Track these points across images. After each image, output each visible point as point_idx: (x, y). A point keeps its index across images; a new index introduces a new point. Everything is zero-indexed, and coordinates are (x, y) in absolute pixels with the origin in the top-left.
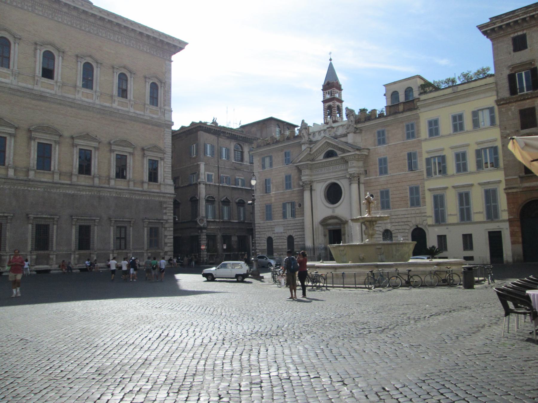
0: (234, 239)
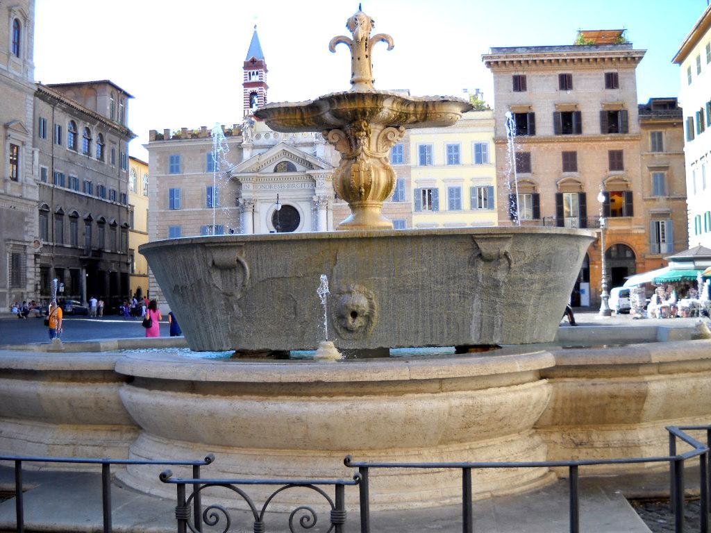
0: (67, 274)
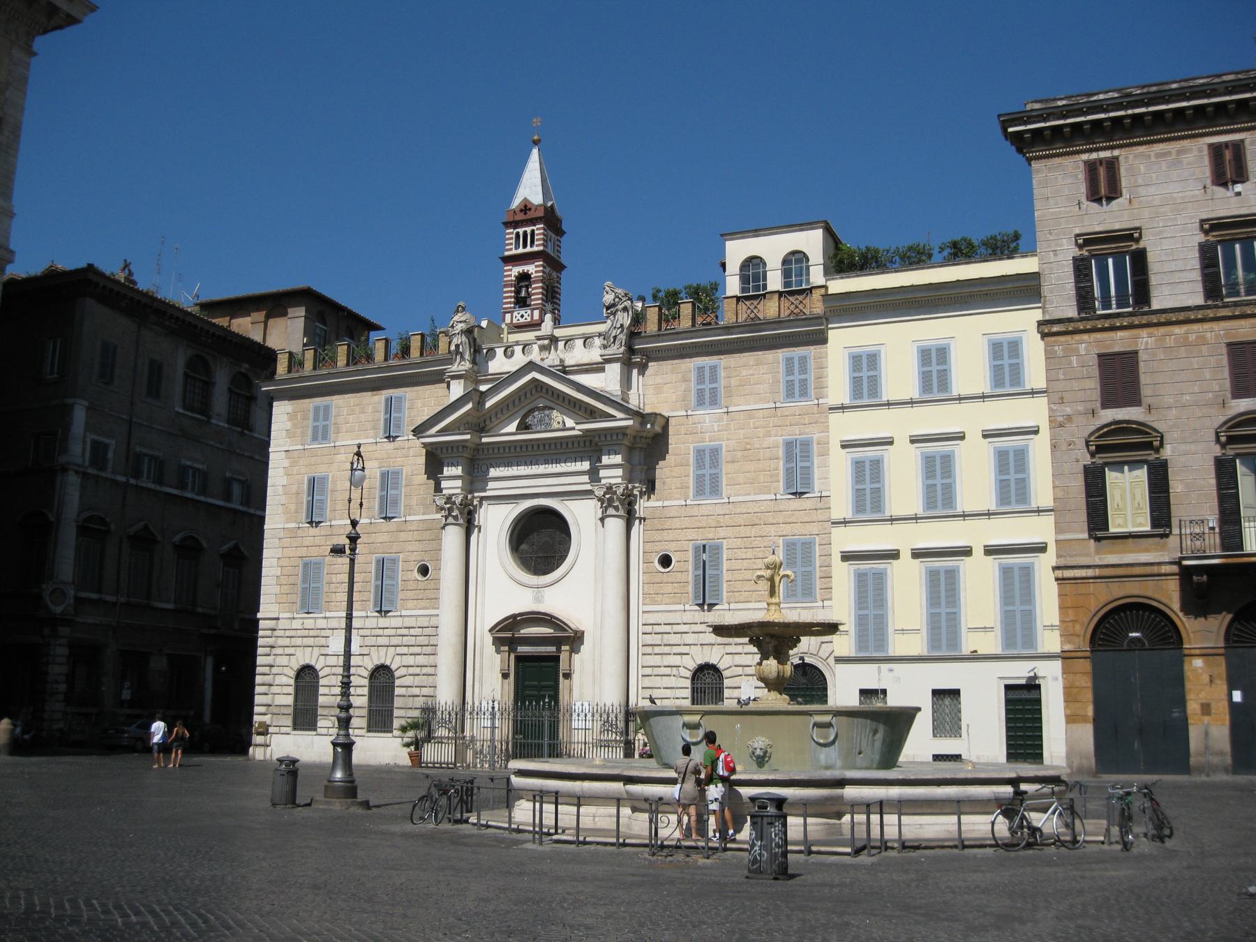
0: (158, 664)
